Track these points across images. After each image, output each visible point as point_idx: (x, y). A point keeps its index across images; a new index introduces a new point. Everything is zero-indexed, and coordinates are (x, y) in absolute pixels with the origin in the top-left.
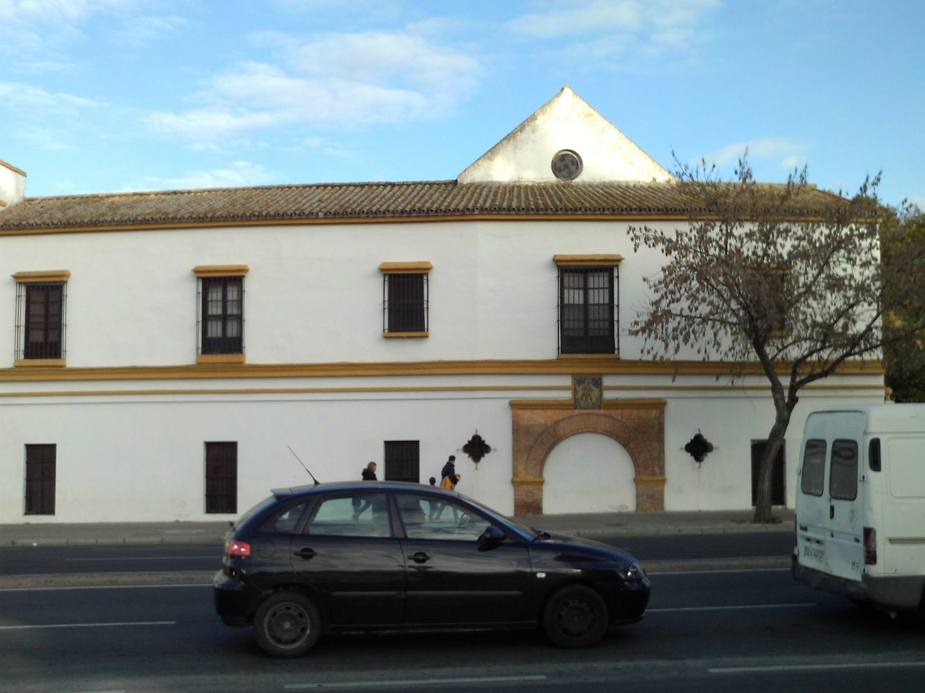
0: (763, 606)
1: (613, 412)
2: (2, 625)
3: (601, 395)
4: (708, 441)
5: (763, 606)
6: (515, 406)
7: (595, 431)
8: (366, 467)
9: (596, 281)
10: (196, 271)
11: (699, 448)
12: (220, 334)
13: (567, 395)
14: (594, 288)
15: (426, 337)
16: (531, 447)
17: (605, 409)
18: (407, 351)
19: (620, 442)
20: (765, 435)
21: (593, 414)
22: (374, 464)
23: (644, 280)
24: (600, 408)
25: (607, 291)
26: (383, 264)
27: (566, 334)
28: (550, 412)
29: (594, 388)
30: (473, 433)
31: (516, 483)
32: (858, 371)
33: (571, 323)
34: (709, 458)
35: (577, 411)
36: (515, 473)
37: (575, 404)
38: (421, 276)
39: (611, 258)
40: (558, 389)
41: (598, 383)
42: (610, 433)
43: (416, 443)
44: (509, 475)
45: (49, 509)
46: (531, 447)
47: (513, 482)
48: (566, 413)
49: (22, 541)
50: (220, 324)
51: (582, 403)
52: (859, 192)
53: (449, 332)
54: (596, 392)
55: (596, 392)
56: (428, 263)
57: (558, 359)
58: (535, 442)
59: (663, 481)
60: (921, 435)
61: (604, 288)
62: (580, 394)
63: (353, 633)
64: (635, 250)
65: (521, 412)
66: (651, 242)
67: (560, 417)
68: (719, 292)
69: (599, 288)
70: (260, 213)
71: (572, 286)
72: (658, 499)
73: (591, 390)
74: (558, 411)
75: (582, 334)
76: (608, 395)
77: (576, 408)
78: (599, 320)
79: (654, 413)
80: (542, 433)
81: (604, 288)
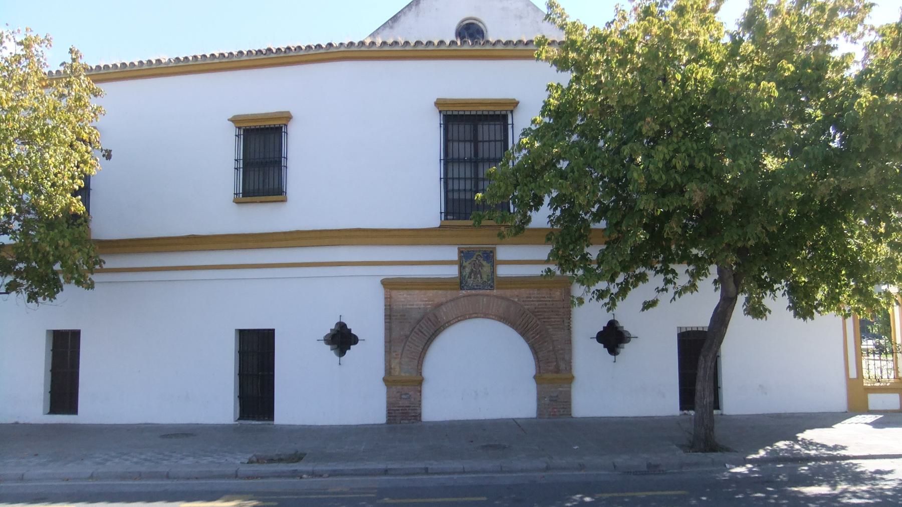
0: (447, 499)
1: (508, 293)
3: (493, 272)
4: (625, 329)
5: (447, 499)
6: (389, 284)
7: (486, 316)
8: (554, 68)
9: (486, 131)
10: (440, 104)
11: (342, 339)
12: (480, 127)
13: (452, 272)
15: (284, 201)
16: (407, 337)
17: (498, 288)
18: (262, 218)
19: (516, 329)
22: (837, 48)
23: (71, 51)
24: (492, 288)
26: (438, 99)
28: (431, 293)
29: (484, 263)
31: (389, 380)
33: (462, 182)
34: (329, 326)
36: (388, 370)
37: (461, 283)
38: (245, 194)
39: (473, 110)
41: (489, 256)
42: (504, 319)
44: (382, 373)
45: (72, 408)
47: (385, 380)
48: (450, 294)
50: (480, 155)
51: (470, 281)
53: (315, 191)
54: (487, 268)
55: (487, 268)
56: (288, 112)
57: (441, 227)
58: (413, 331)
59: (570, 379)
61: (483, 141)
62: (468, 270)
63: (302, 497)
64: (872, 5)
66: (670, 276)
67: (444, 300)
68: (146, 460)
69: (489, 141)
70: (705, 107)
71: (462, 138)
72: (565, 402)
73: (481, 265)
74: (440, 292)
76: (503, 271)
77: (462, 288)
80: (419, 321)
81: (483, 141)
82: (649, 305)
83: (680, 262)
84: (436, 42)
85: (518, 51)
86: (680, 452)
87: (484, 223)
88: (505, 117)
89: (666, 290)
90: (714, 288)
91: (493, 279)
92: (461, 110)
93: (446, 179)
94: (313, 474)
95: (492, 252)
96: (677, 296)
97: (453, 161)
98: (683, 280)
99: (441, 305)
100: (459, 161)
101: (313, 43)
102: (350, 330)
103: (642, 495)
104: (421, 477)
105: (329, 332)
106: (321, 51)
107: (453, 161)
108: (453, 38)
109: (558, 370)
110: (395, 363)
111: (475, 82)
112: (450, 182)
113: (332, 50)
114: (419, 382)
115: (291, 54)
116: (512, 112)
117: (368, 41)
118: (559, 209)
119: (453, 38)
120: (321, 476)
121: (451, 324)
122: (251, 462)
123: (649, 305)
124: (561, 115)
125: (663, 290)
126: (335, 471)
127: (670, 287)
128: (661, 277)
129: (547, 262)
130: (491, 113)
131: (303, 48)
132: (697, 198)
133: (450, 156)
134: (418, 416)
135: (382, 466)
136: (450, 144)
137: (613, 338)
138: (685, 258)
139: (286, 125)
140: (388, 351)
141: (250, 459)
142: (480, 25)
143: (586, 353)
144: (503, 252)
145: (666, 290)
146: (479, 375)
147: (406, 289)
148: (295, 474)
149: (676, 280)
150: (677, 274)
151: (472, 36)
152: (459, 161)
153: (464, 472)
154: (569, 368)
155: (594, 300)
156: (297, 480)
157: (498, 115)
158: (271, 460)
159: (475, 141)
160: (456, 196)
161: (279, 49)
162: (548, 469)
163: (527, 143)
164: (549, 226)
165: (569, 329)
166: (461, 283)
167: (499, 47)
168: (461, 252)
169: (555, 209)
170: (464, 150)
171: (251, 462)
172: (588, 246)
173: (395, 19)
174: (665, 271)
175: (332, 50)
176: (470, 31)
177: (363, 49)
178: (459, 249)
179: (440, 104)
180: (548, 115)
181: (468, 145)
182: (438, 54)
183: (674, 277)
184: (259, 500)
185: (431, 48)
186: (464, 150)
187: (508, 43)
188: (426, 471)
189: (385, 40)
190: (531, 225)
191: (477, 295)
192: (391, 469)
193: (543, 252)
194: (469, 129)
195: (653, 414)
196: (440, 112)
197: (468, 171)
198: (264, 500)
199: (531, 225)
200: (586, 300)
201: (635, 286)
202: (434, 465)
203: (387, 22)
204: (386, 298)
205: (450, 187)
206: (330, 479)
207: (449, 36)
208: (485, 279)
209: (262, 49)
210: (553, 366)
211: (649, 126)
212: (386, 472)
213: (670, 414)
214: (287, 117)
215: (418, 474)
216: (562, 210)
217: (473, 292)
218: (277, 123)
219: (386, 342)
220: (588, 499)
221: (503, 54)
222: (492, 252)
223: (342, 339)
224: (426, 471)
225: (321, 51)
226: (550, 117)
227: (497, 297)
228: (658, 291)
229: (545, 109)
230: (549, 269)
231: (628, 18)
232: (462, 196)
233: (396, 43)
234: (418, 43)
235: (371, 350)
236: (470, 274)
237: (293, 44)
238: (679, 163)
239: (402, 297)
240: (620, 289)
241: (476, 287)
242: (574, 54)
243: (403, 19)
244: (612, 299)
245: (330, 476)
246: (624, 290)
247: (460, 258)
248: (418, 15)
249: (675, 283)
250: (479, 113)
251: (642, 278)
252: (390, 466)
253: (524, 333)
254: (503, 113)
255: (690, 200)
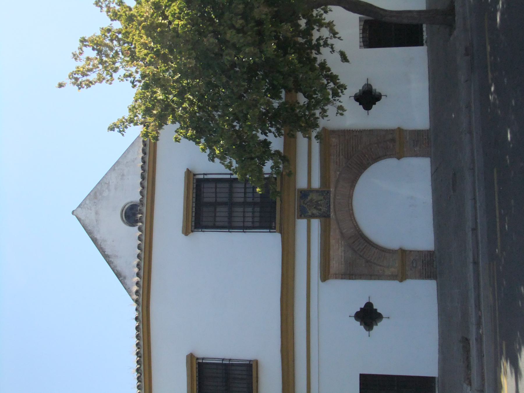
2: (435, 392)
3: (317, 191)
4: (361, 88)
6: (325, 276)
7: (351, 197)
9: (209, 195)
10: (186, 232)
11: (368, 316)
12: (206, 200)
13: (316, 223)
14: (216, 188)
15: (257, 362)
16: (367, 261)
17: (329, 187)
20: (136, 198)
21: (334, 199)
24: (329, 192)
25: (219, 185)
26: (183, 233)
27: (257, 224)
28: (332, 242)
29: (309, 198)
30: (367, 301)
31: (402, 277)
32: (350, 205)
34: (358, 326)
35: (332, 214)
36: (393, 277)
37: (325, 217)
40: (308, 233)
41: (304, 194)
42: (353, 182)
43: (361, 375)
44: (395, 283)
46: (367, 261)
47: (401, 281)
49: (126, 221)
50: (226, 200)
51: (324, 209)
52: (99, 33)
54: (314, 197)
56: (187, 356)
57: (281, 232)
60: (147, 391)
62: (315, 212)
63: (497, 315)
64: (112, 129)
65: (332, 271)
66: (322, 42)
67: (337, 231)
72: (417, 135)
73: (311, 200)
75: (257, 209)
76: (316, 184)
77: (329, 216)
78: (245, 193)
79: (334, 140)
81: (216, 188)
82: (344, 58)
83: (311, 35)
84: (139, 251)
85: (149, 149)
86: (456, 33)
87: (278, 189)
88: (199, 181)
89: (332, 45)
90: (329, 12)
91: (322, 191)
92: (192, 215)
93: (244, 228)
94: (479, 324)
95: (301, 192)
96: (337, 36)
97: (230, 222)
98: (325, 32)
99: (342, 233)
100: (230, 216)
101: (135, 332)
102: (360, 104)
103: (489, 48)
104: (479, 235)
105: (362, 327)
106: (141, 327)
107: (230, 222)
108: (136, 228)
109: (393, 140)
110: (388, 272)
111: (171, 204)
112: (247, 224)
113: (141, 318)
114: (403, 253)
115: (142, 352)
116: (195, 175)
117: (135, 297)
118: (270, 128)
119: (136, 228)
120: (480, 317)
121: (357, 225)
122: (470, 384)
123: (344, 58)
124: (201, 129)
125: (332, 48)
126: (476, 306)
127: (330, 42)
128: (322, 49)
129: (309, 138)
130: (195, 191)
131: (138, 341)
132: (266, 10)
133: (226, 224)
134: (430, 253)
135: (471, 267)
136: (217, 224)
137: (368, 98)
138: (307, 33)
139: (197, 359)
140: (379, 277)
141: (468, 385)
142: (126, 207)
143: (380, 118)
144: (302, 183)
145: (332, 45)
146: (397, 203)
147: (329, 262)
148: (479, 339)
149: (325, 37)
150: (320, 37)
151: (135, 215)
152: (230, 216)
153: (475, 199)
154: (392, 131)
155: (340, 99)
156: (484, 338)
157: (196, 195)
158: (468, 367)
159: (215, 204)
160: (257, 219)
161: (138, 362)
162: (470, 133)
163: (219, 150)
164: (283, 137)
165: (361, 131)
166: (325, 217)
167: (146, 184)
168: (300, 217)
169: (270, 131)
170: (222, 212)
171: (470, 384)
172: (299, 103)
173: (119, 275)
174: (317, 47)
175: (141, 318)
176: (131, 215)
177: (141, 292)
178: (298, 218)
179: (186, 232)
180: (200, 139)
181: (218, 209)
182: (146, 277)
183: (322, 39)
184: (501, 359)
185: (143, 238)
186: (222, 212)
187: (143, 177)
188: (475, 230)
189: (135, 275)
190: (282, 150)
191: (334, 203)
192: (474, 259)
193: (302, 141)
194: (208, 207)
195: (437, 368)
196: (192, 231)
197: (238, 210)
198: (501, 354)
199: (282, 150)
200: (340, 104)
201: (329, 69)
202: (469, 224)
203: (120, 281)
204: (336, 278)
205: (250, 224)
206: (482, 308)
207: (134, 232)
208: (322, 198)
209: (136, 377)
210: (391, 144)
211: (209, 41)
212: (476, 263)
213: (426, 53)
214: (191, 358)
215: (477, 236)
216: (271, 127)
217: (332, 207)
218: (195, 366)
219: (371, 279)
220: (493, 89)
221: (150, 179)
222: (301, 192)
223: (368, 316)
224: (475, 230)
225: (141, 327)
226: (200, 138)
227: (336, 188)
228: (334, 51)
229: (195, 139)
230: (315, 137)
231: (130, 72)
232: (257, 214)
233: (138, 265)
234: (139, 247)
235: (380, 292)
236: (317, 209)
237: (134, 349)
238: (239, 22)
239: (335, 265)
240: (331, 81)
241: (329, 205)
242: (155, 111)
243: (119, 268)
244: (338, 87)
245: (480, 309)
246: (333, 78)
247: (305, 217)
248: (116, 256)
249: (327, 38)
250: (194, 200)
251: (323, 66)
252: (471, 259)
253: (363, 167)
254: (195, 181)
255: (266, 14)
